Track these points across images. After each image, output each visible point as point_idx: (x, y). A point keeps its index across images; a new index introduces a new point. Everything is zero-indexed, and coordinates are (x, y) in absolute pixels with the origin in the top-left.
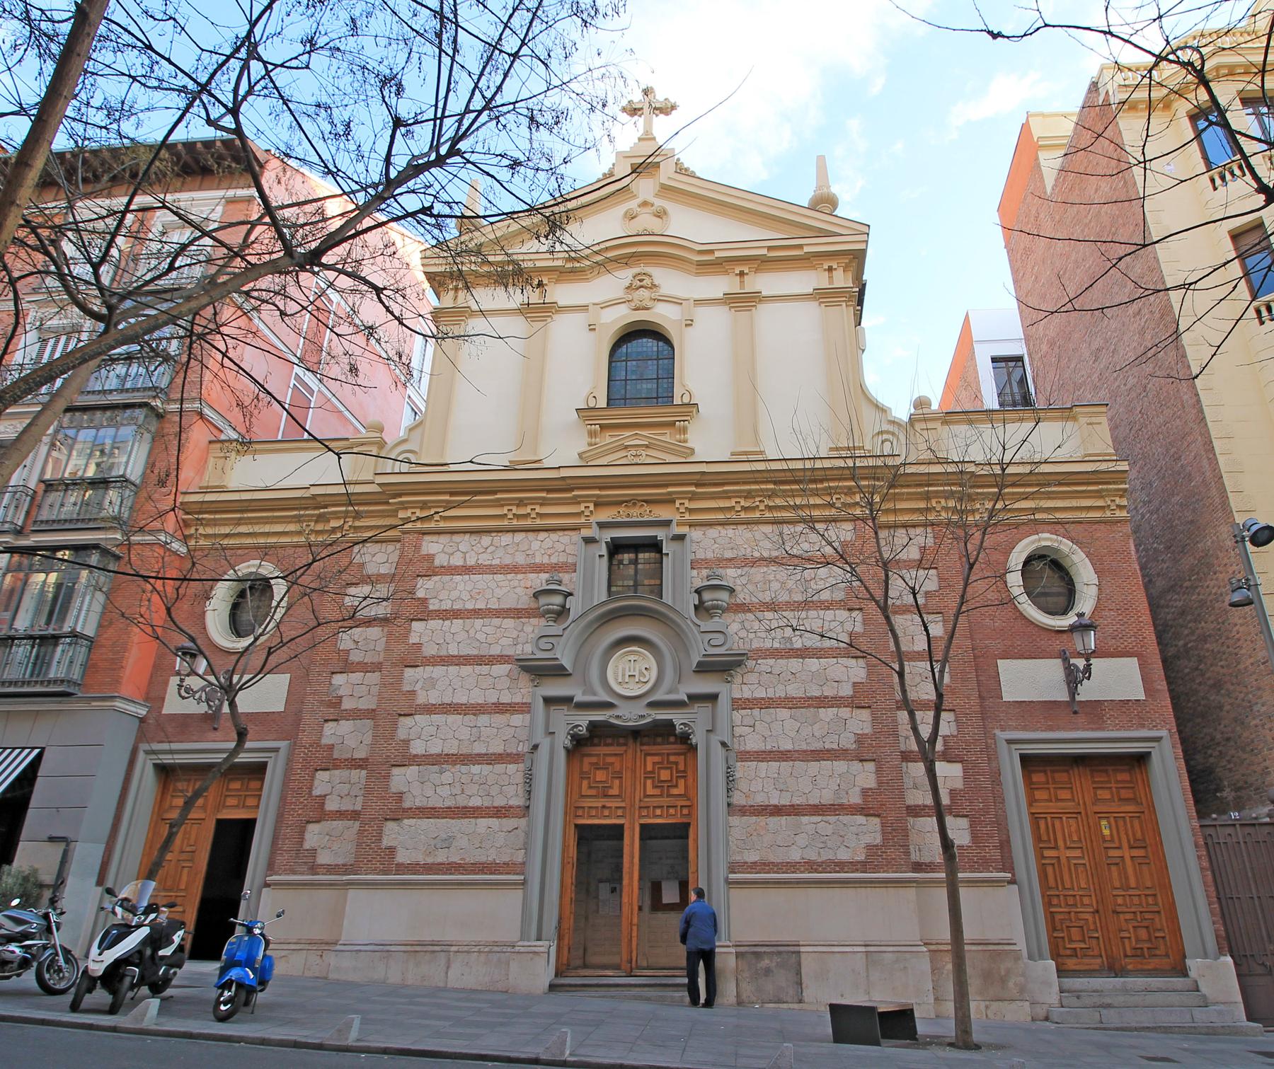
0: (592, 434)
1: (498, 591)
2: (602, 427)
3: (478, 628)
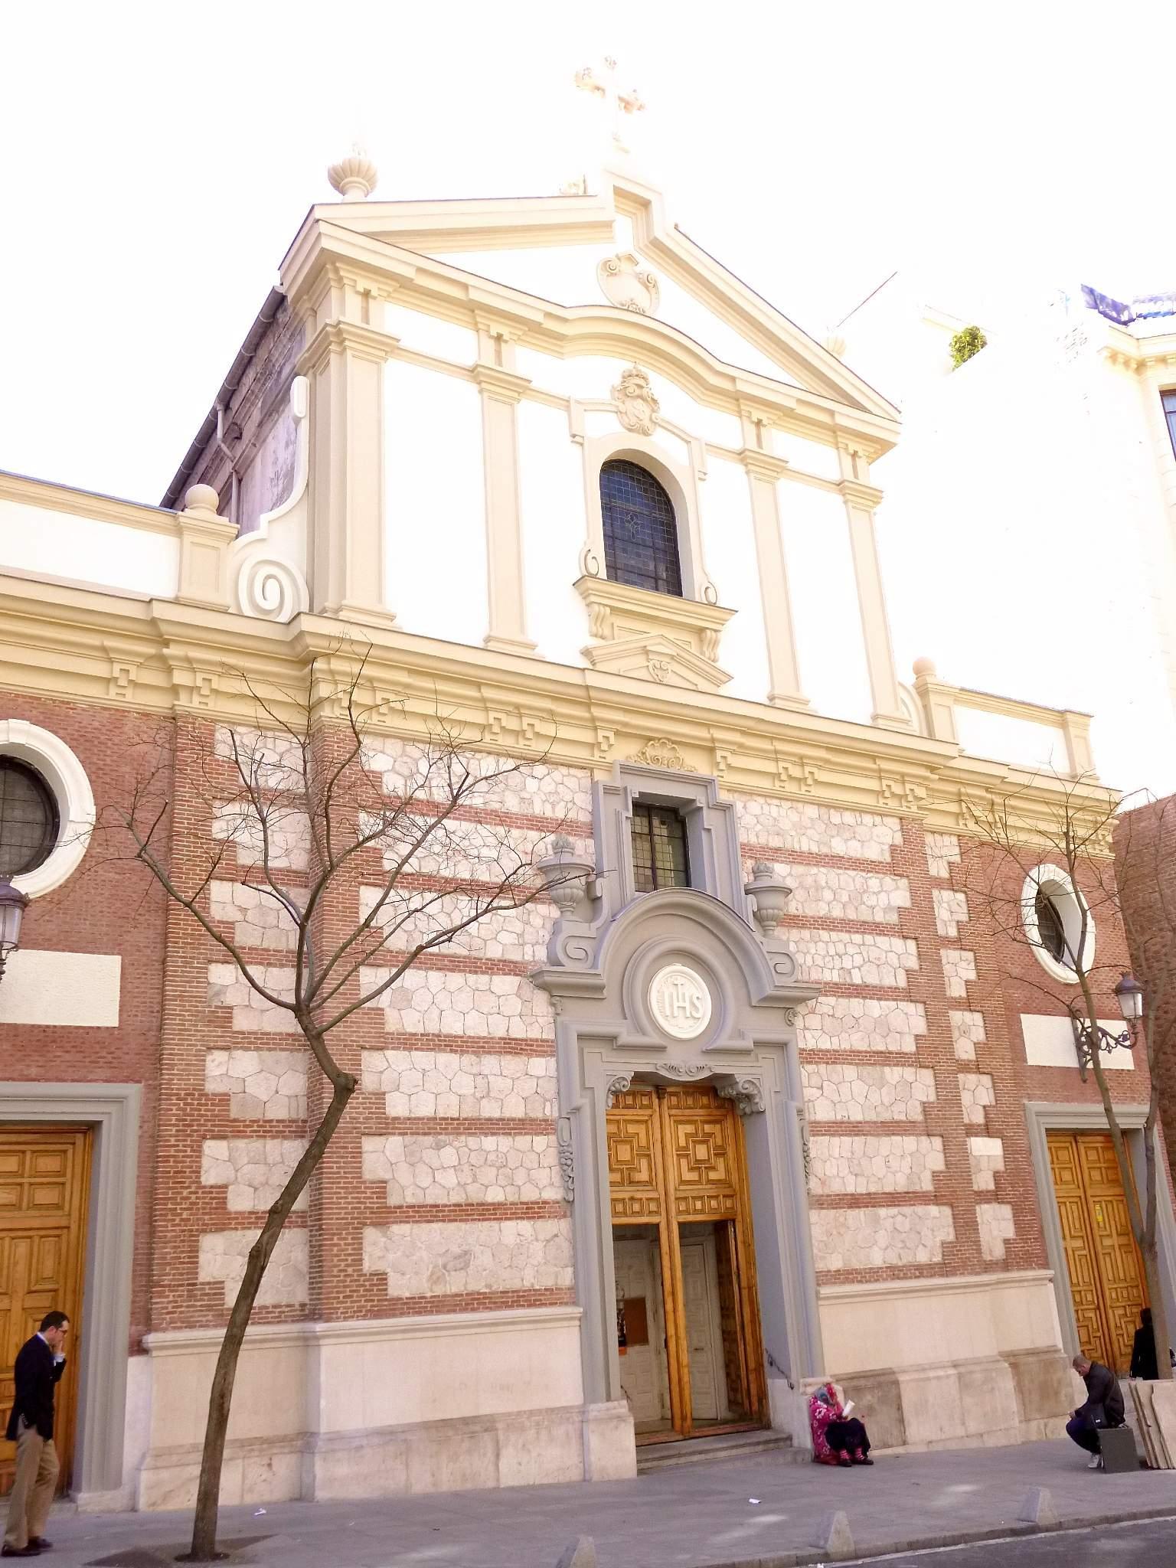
0: (598, 619)
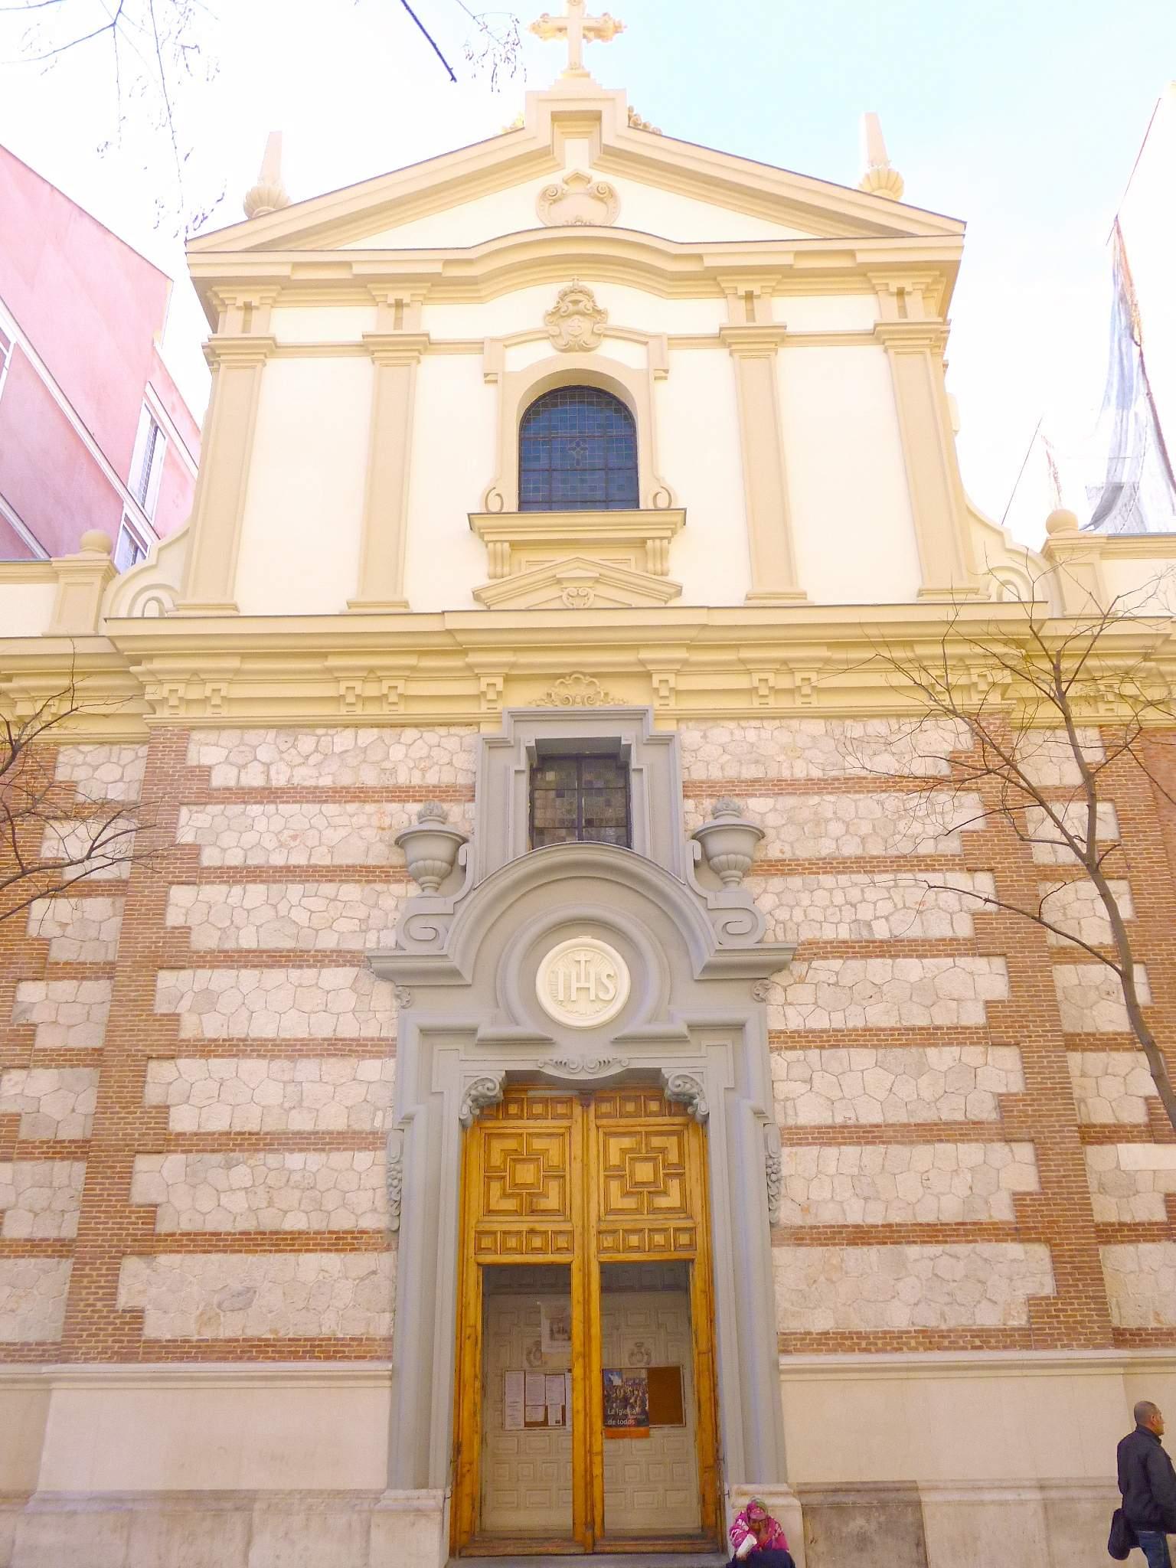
0: (495, 558)
1: (329, 832)
2: (514, 544)
3: (295, 901)
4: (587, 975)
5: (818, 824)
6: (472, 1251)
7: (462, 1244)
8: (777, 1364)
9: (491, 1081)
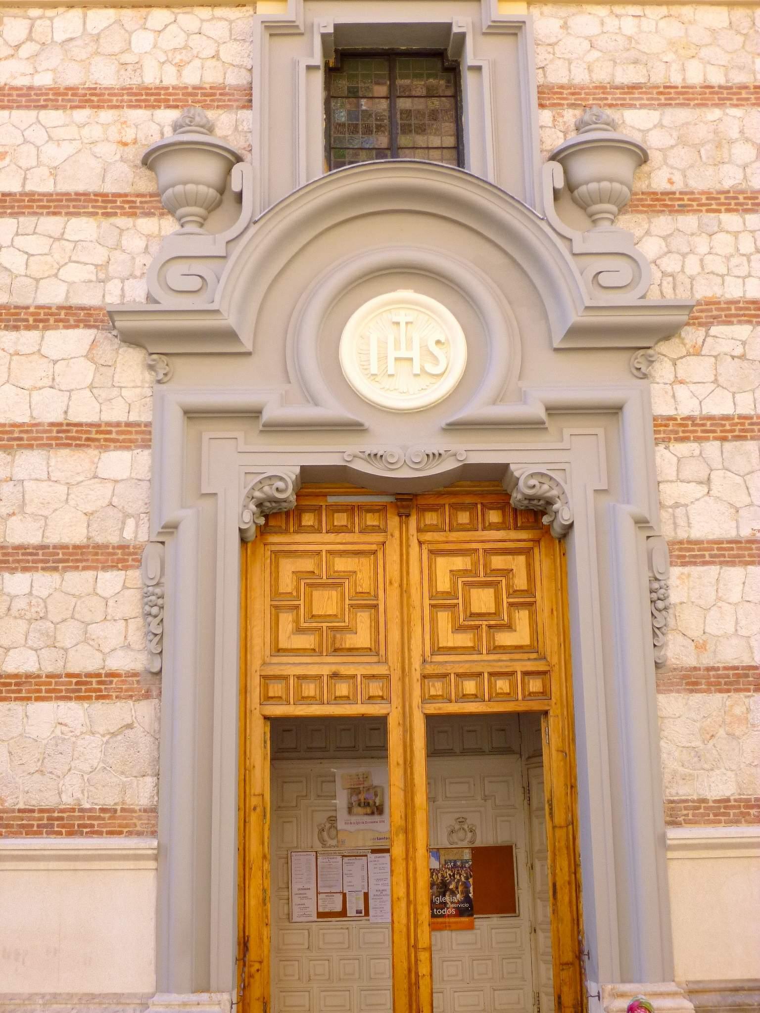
4: (409, 341)
5: (719, 146)
6: (256, 700)
7: (244, 691)
8: (663, 838)
9: (281, 479)
